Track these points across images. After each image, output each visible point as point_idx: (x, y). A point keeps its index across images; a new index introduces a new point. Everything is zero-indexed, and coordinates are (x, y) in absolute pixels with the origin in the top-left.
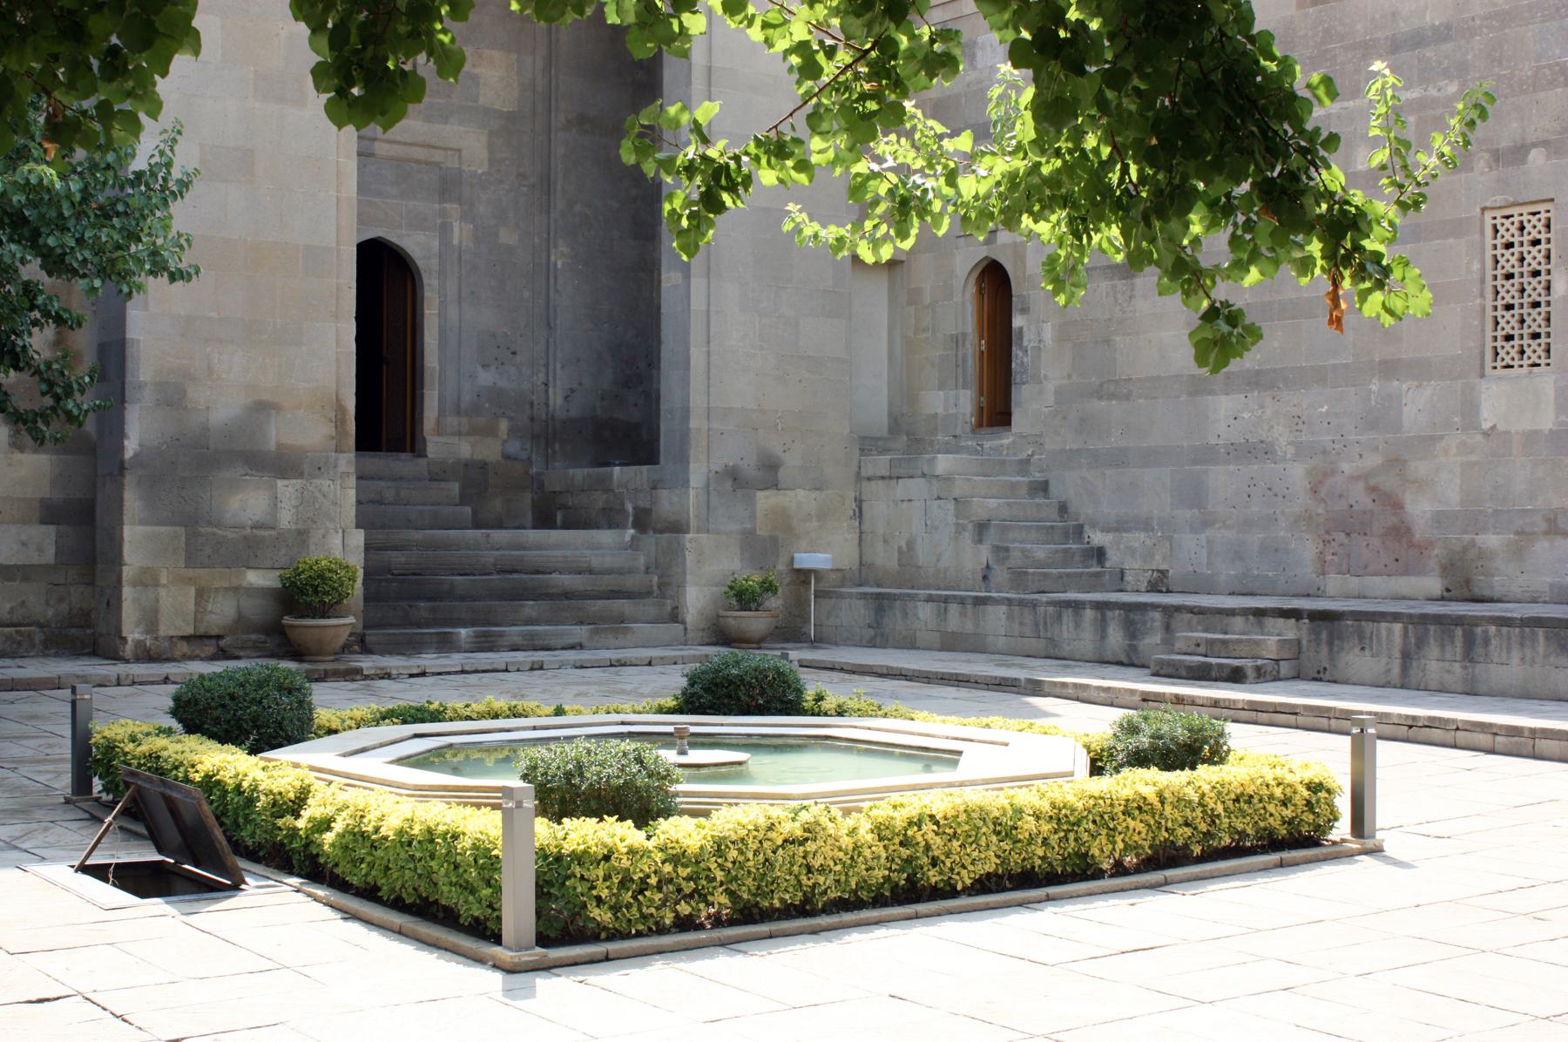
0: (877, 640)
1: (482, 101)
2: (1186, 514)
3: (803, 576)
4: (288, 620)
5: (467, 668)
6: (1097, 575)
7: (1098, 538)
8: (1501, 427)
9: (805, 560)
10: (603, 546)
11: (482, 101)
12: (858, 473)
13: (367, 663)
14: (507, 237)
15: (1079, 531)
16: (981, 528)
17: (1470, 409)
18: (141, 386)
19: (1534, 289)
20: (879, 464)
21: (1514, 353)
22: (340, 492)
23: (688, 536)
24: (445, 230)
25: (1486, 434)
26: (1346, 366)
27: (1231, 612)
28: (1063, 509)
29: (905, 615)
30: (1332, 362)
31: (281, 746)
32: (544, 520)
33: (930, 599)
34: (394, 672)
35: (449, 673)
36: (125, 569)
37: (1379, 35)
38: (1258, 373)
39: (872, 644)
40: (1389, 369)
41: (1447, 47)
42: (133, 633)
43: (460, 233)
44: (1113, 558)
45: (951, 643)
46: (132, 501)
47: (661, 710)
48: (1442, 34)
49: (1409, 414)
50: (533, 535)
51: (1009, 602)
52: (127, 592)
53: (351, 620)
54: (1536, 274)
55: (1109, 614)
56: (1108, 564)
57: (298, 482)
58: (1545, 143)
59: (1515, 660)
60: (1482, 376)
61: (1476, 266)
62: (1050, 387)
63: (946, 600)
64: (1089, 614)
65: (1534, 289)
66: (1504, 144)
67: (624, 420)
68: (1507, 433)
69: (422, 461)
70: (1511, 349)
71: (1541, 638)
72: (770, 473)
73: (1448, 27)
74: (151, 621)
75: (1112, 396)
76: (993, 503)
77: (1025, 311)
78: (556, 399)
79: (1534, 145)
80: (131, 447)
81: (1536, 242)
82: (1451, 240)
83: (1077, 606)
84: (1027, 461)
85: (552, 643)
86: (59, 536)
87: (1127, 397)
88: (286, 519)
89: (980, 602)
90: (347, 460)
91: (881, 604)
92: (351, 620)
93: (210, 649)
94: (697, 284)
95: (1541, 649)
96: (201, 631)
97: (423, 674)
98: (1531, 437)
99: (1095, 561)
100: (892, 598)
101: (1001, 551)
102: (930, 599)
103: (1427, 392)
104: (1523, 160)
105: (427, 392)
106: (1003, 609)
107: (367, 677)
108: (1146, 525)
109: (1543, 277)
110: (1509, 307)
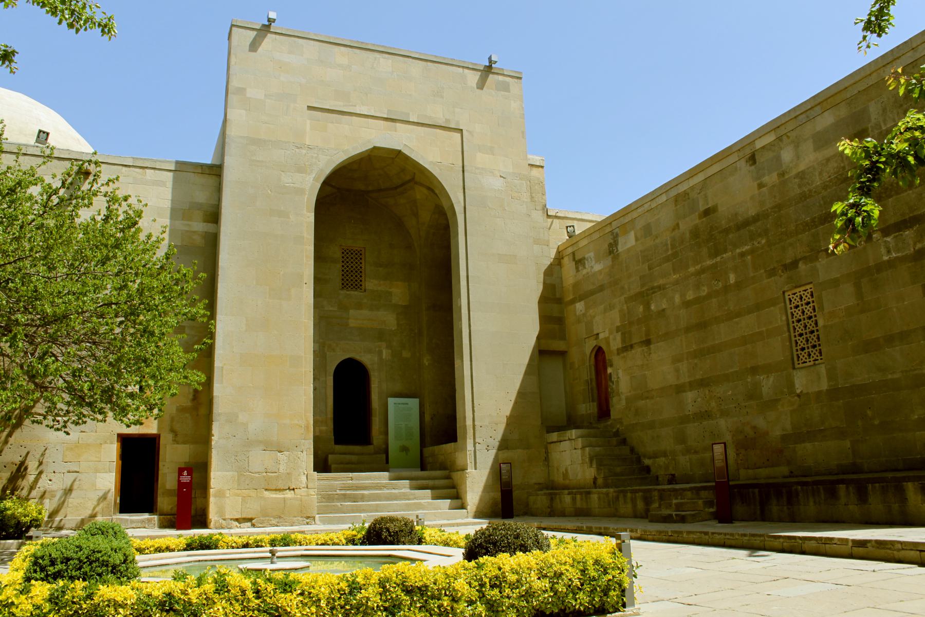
1: (393, 302)
2: (679, 447)
7: (647, 462)
8: (805, 392)
11: (393, 302)
14: (406, 354)
17: (791, 385)
18: (219, 415)
19: (810, 324)
21: (806, 356)
24: (380, 353)
25: (799, 396)
26: (736, 372)
27: (684, 490)
28: (632, 450)
29: (561, 501)
30: (731, 370)
36: (211, 490)
37: (731, 224)
38: (702, 380)
40: (754, 370)
41: (759, 224)
43: (386, 353)
44: (653, 470)
47: (352, 541)
48: (756, 219)
49: (765, 390)
52: (212, 500)
54: (810, 318)
58: (804, 258)
59: (811, 503)
60: (794, 368)
61: (784, 318)
62: (623, 397)
64: (629, 495)
65: (810, 324)
66: (788, 261)
68: (808, 393)
69: (371, 447)
70: (804, 355)
71: (822, 491)
73: (758, 215)
75: (647, 398)
79: (800, 259)
81: (808, 303)
82: (772, 308)
85: (768, 544)
86: (159, 520)
87: (652, 398)
88: (282, 468)
93: (249, 524)
95: (823, 496)
96: (244, 516)
98: (819, 393)
100: (556, 494)
103: (771, 379)
104: (797, 267)
105: (373, 418)
108: (665, 454)
109: (814, 319)
110: (801, 335)
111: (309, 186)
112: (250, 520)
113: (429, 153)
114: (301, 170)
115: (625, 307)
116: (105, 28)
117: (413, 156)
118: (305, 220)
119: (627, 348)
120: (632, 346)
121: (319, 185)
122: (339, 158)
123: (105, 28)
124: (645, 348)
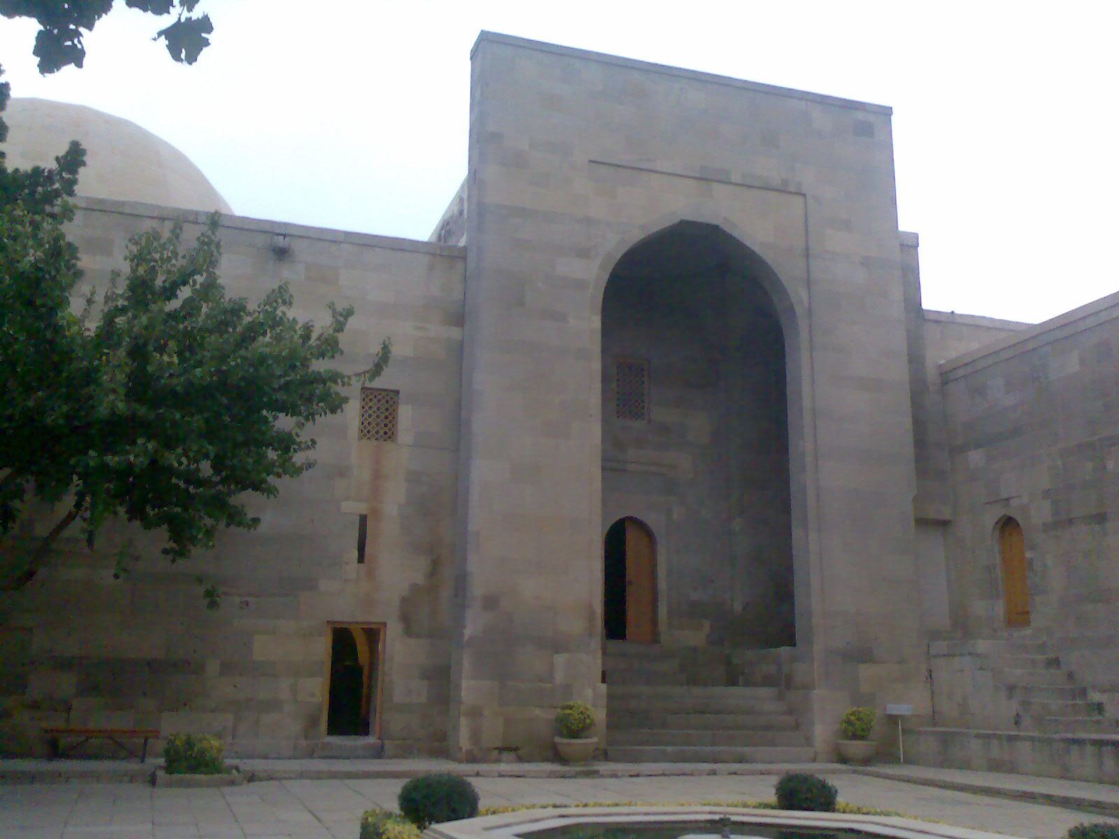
0: (943, 764)
3: (893, 720)
4: (558, 739)
5: (666, 773)
6: (1098, 722)
7: (1096, 697)
9: (895, 709)
10: (762, 698)
12: (928, 653)
13: (604, 767)
15: (1083, 692)
16: (1011, 689)
20: (941, 646)
22: (590, 660)
23: (815, 692)
28: (1070, 676)
31: (795, 810)
32: (732, 681)
33: (977, 736)
34: (620, 774)
35: (655, 775)
39: (941, 765)
42: (464, 742)
45: (995, 766)
46: (467, 663)
50: (719, 690)
51: (1032, 739)
53: (595, 740)
55: (1104, 748)
56: (1107, 715)
57: (566, 655)
63: (988, 736)
67: (772, 619)
72: (864, 655)
74: (475, 736)
76: (1019, 672)
77: (1032, 548)
78: (738, 607)
80: (468, 632)
83: (1080, 742)
84: (1044, 644)
89: (1011, 739)
90: (596, 642)
91: (946, 740)
92: (595, 740)
93: (512, 755)
94: (813, 536)
97: (638, 776)
99: (1096, 712)
101: (1026, 704)
102: (977, 736)
106: (1028, 744)
107: (602, 776)
111: (592, 274)
112: (516, 749)
113: (756, 227)
114: (584, 253)
115: (1059, 463)
116: (155, 39)
117: (736, 234)
118: (587, 324)
119: (1063, 522)
120: (1071, 522)
121: (606, 277)
122: (636, 236)
123: (155, 39)
124: (1097, 528)
